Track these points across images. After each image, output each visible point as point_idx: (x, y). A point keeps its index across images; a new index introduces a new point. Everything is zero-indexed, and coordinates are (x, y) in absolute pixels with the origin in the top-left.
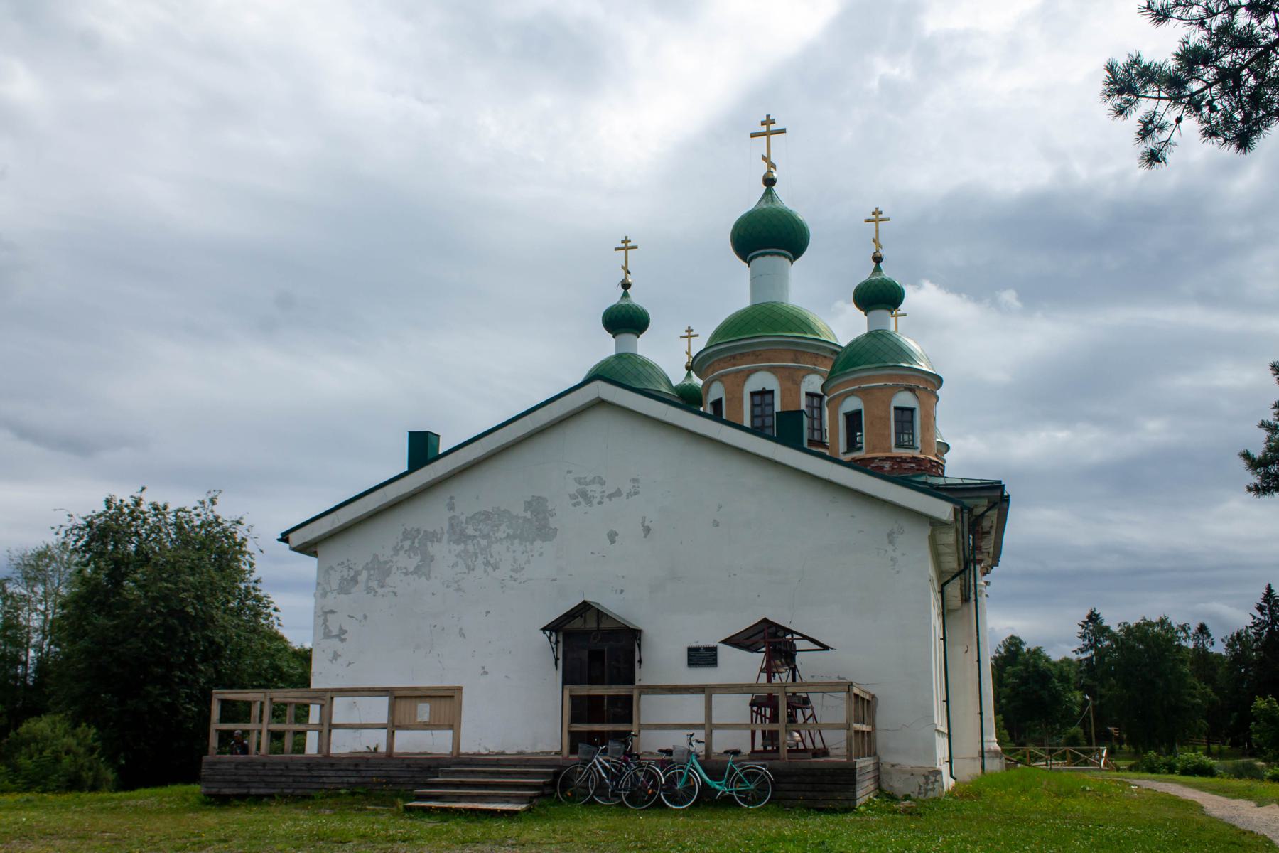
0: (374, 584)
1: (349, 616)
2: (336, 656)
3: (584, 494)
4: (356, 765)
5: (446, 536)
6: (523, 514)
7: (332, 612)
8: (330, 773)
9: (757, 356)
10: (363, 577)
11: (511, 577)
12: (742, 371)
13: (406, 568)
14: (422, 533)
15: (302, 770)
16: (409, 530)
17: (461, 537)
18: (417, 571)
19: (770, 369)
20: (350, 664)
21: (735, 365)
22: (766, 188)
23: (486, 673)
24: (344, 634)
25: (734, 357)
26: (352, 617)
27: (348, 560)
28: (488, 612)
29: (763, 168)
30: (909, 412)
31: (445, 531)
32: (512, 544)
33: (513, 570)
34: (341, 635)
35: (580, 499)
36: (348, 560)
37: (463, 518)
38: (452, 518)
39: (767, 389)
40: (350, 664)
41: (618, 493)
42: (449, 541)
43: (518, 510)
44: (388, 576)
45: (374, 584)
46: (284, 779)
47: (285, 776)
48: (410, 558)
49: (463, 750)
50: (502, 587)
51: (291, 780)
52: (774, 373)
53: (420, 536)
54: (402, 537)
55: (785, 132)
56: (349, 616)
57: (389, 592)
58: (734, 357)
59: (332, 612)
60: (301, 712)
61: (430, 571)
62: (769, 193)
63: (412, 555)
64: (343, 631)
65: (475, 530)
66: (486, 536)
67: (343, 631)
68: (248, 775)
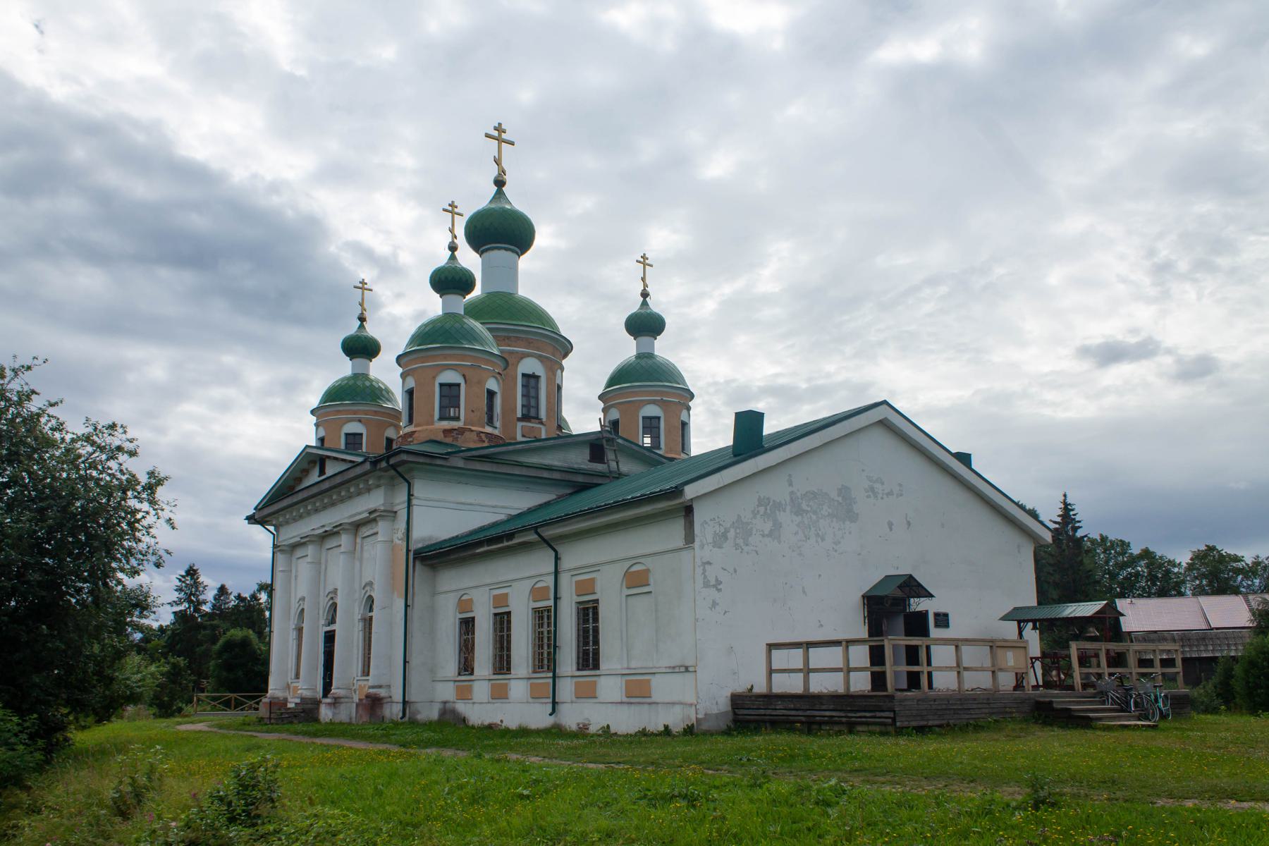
0: (740, 542)
1: (722, 568)
2: (714, 604)
3: (872, 489)
4: (988, 699)
5: (788, 508)
6: (836, 498)
7: (709, 563)
8: (975, 706)
9: (529, 343)
10: (731, 534)
11: (833, 548)
12: (517, 352)
13: (762, 531)
14: (771, 501)
15: (956, 704)
16: (762, 497)
17: (799, 512)
18: (770, 535)
19: (540, 358)
20: (726, 612)
21: (509, 346)
22: (496, 188)
23: (822, 626)
24: (719, 584)
25: (509, 338)
26: (725, 570)
27: (718, 517)
28: (820, 576)
29: (494, 171)
30: (657, 420)
31: (788, 503)
32: (832, 521)
33: (834, 543)
34: (717, 585)
35: (870, 493)
36: (718, 517)
37: (799, 494)
38: (792, 493)
39: (536, 374)
40: (726, 612)
41: (890, 494)
42: (791, 512)
43: (834, 495)
44: (751, 535)
45: (740, 542)
46: (948, 712)
47: (802, 710)
48: (765, 522)
49: (853, 689)
50: (828, 556)
51: (952, 712)
52: (542, 362)
53: (771, 504)
54: (757, 503)
55: (513, 145)
56: (722, 568)
57: (752, 550)
58: (509, 338)
59: (709, 563)
60: (595, 651)
61: (780, 536)
62: (500, 194)
63: (766, 519)
64: (718, 582)
65: (808, 506)
66: (815, 513)
67: (718, 582)
68: (776, 709)
